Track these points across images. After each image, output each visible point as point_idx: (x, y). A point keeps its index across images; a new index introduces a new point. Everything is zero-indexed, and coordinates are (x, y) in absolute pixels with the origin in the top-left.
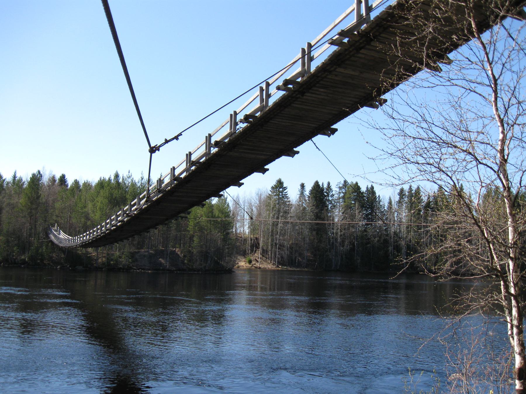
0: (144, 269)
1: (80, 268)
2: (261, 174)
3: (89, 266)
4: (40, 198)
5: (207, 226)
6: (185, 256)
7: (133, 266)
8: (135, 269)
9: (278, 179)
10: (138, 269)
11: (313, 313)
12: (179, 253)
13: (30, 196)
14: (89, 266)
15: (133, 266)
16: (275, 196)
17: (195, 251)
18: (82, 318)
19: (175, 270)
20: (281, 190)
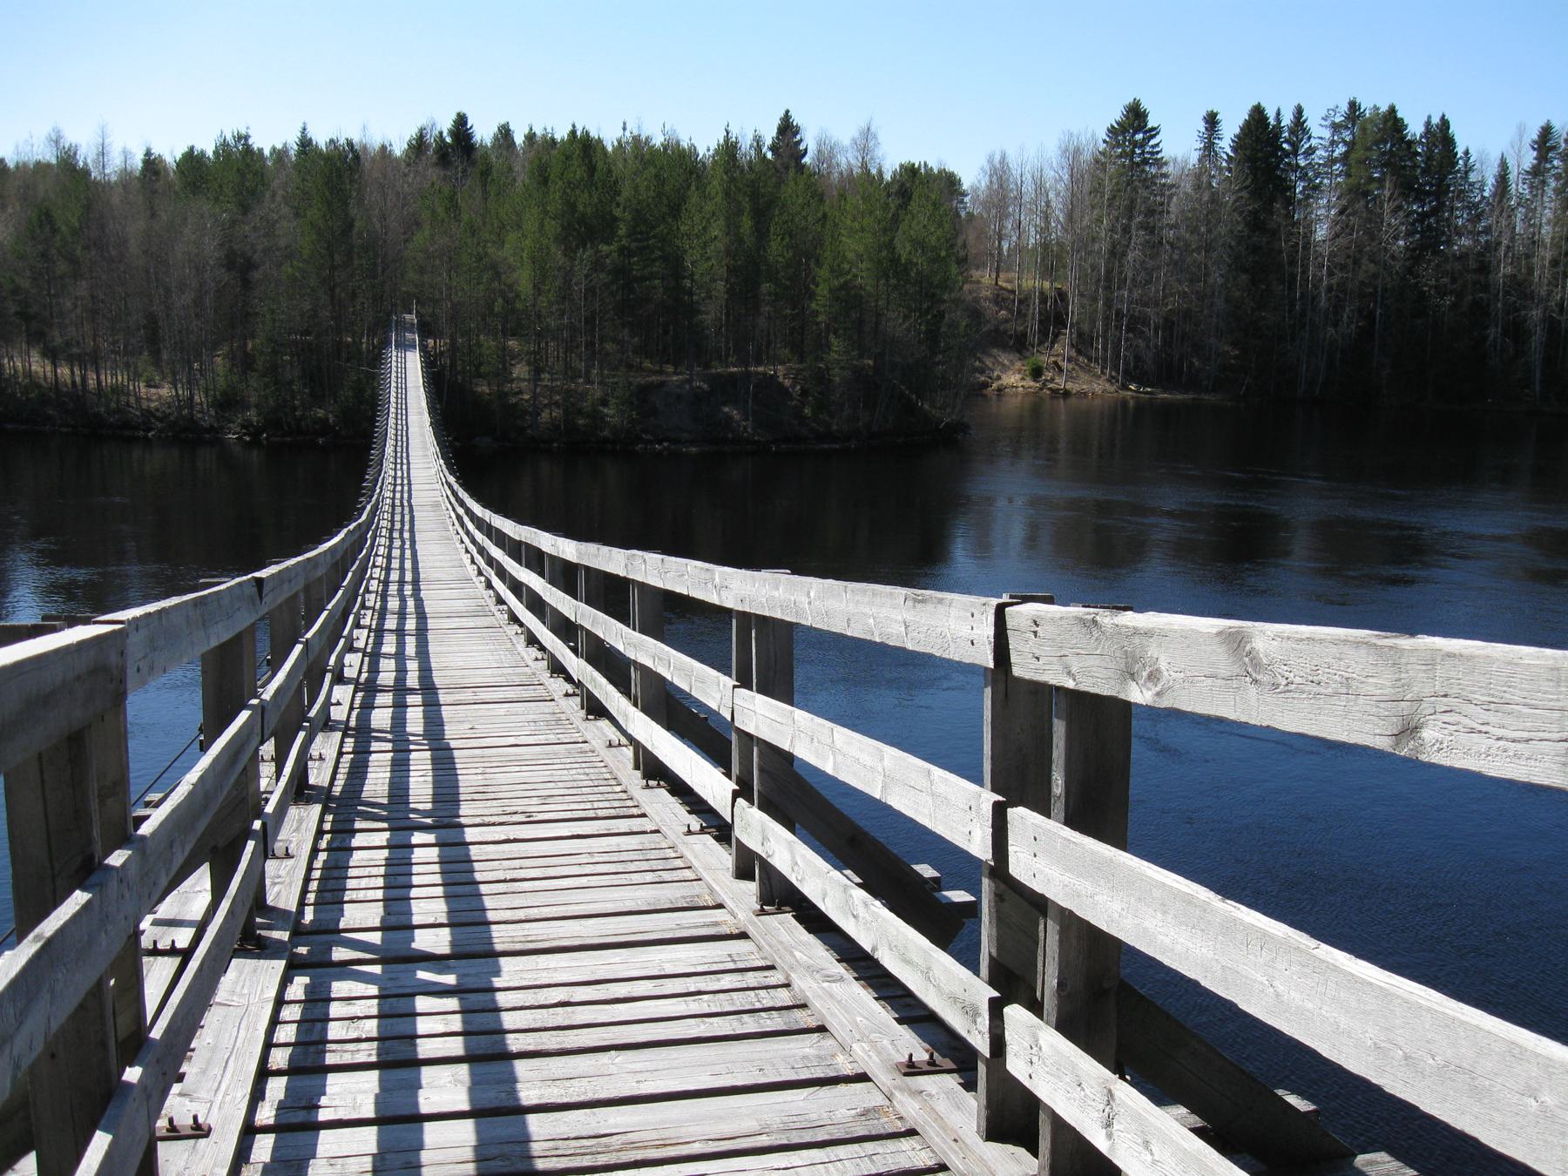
6: (804, 392)
12: (787, 383)
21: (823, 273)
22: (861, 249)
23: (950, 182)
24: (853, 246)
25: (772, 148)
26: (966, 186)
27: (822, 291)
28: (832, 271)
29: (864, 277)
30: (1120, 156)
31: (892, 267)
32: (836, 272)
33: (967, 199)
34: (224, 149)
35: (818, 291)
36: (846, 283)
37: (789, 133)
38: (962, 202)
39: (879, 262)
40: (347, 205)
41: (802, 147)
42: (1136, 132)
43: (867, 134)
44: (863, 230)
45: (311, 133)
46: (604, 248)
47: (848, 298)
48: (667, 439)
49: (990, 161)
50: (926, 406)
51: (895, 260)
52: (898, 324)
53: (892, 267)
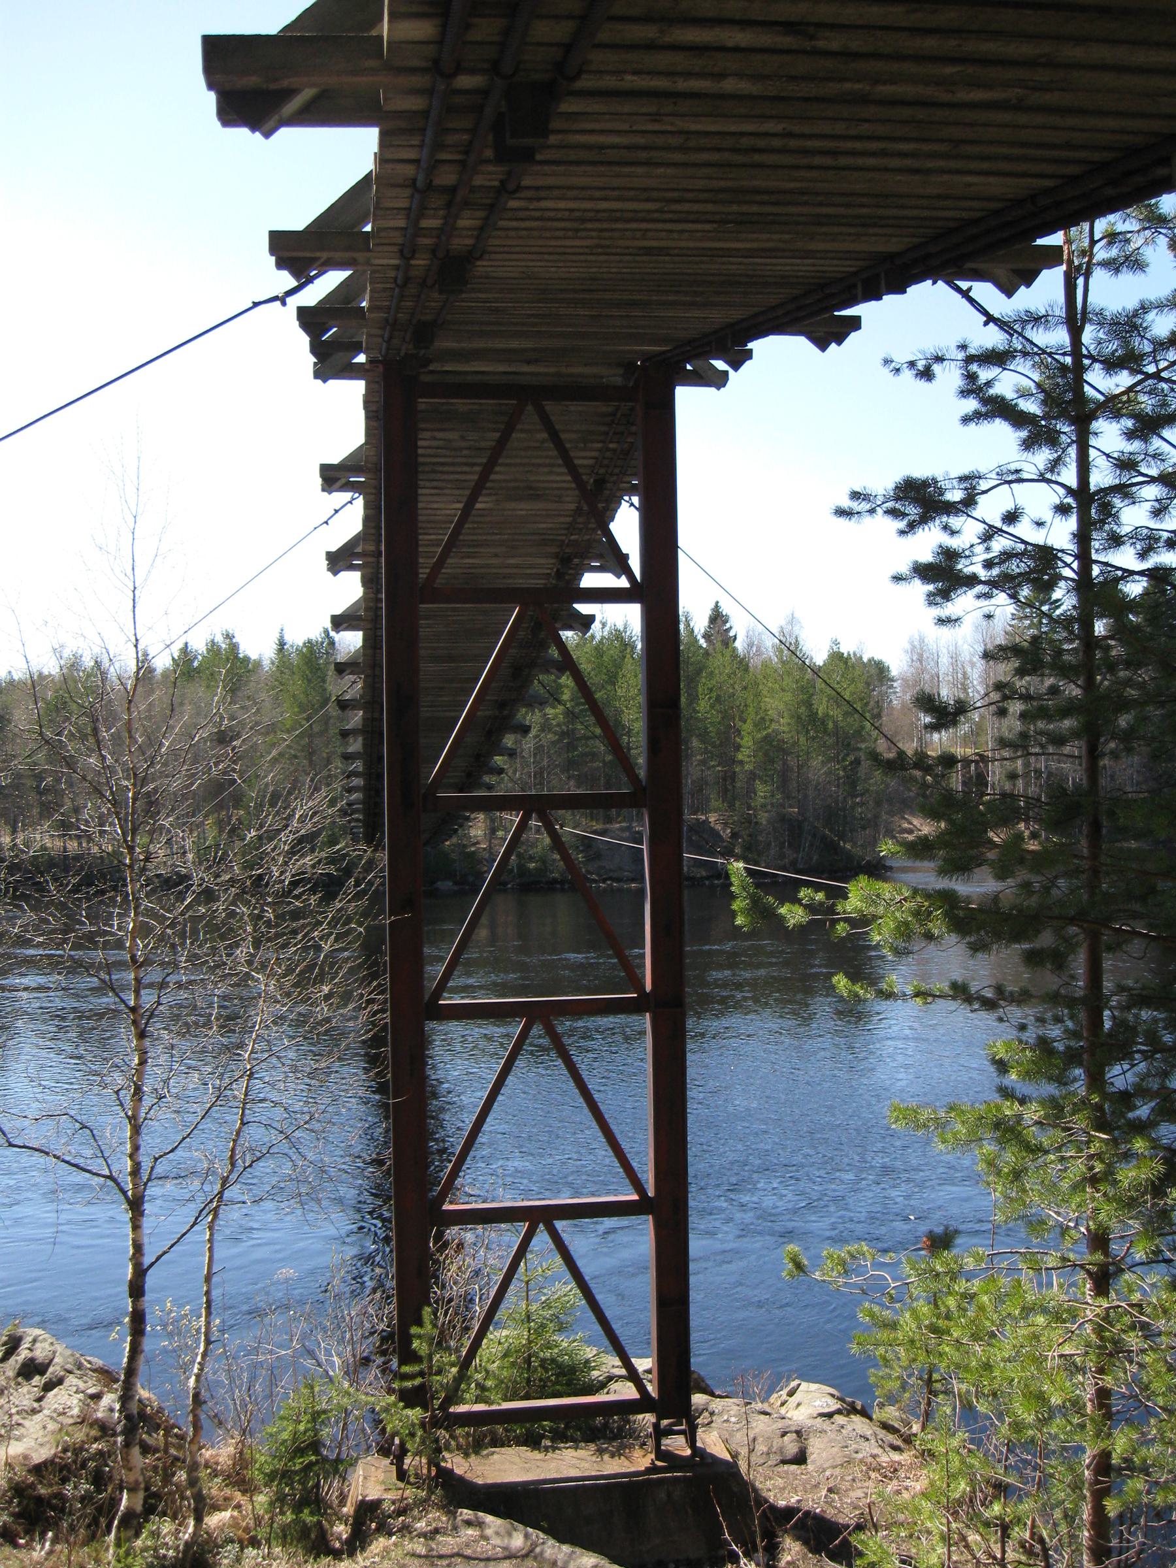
0: (618, 880)
1: (446, 885)
2: (334, 549)
3: (471, 879)
4: (75, 703)
5: (796, 743)
6: (734, 835)
7: (588, 872)
8: (595, 881)
9: (324, 556)
10: (604, 881)
11: (140, 1100)
12: (718, 827)
13: (305, 701)
14: (471, 879)
15: (588, 872)
16: (1029, 627)
17: (763, 818)
18: (982, 972)
19: (708, 878)
20: (1045, 608)
21: (747, 727)
22: (782, 707)
23: (879, 671)
24: (778, 707)
25: (706, 636)
26: (894, 672)
27: (747, 742)
28: (755, 725)
29: (783, 726)
30: (1029, 627)
31: (810, 721)
32: (760, 724)
33: (895, 684)
34: (331, 341)
35: (743, 743)
36: (768, 736)
37: (719, 621)
38: (891, 687)
39: (799, 717)
40: (324, 681)
41: (732, 634)
42: (1042, 604)
43: (792, 620)
44: (783, 690)
45: (288, 638)
46: (550, 711)
47: (772, 748)
48: (610, 878)
49: (912, 643)
50: (848, 846)
51: (813, 716)
52: (818, 767)
53: (810, 721)
